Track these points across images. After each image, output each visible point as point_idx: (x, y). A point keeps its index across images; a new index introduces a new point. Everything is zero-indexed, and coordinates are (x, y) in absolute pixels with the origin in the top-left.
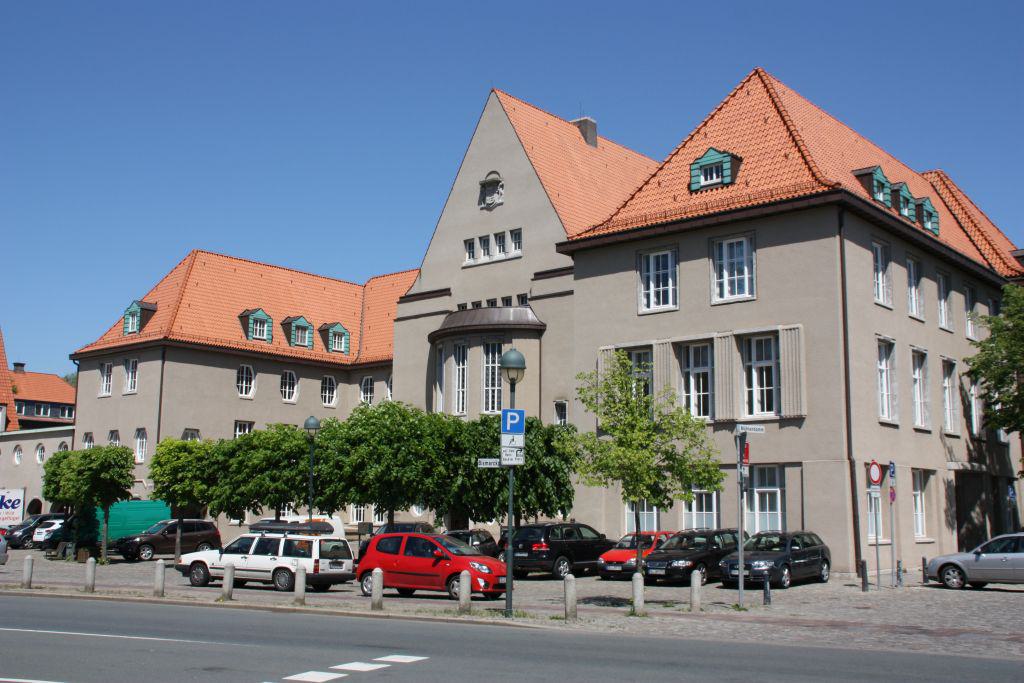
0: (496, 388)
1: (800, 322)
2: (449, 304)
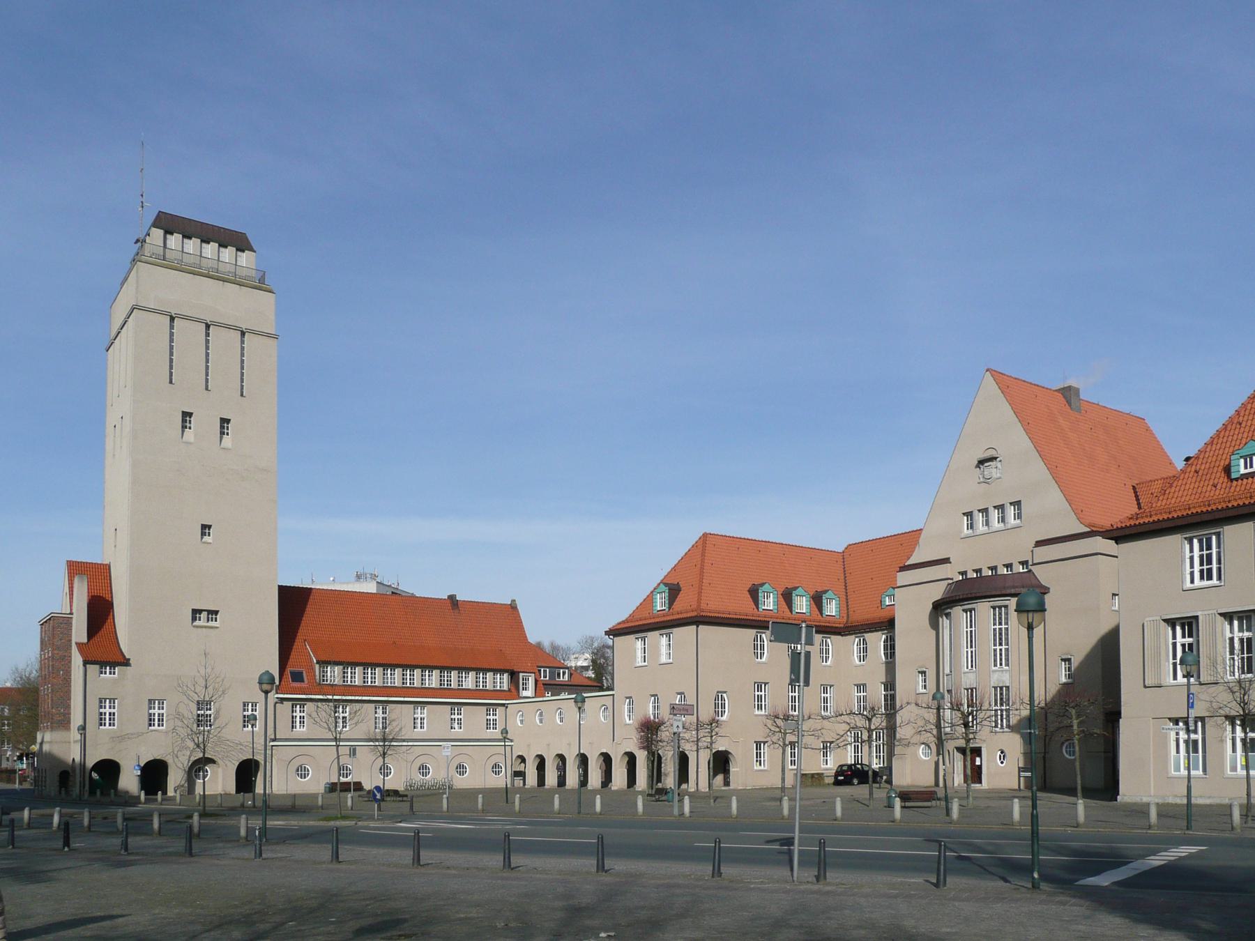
0: (1004, 647)
2: (951, 572)
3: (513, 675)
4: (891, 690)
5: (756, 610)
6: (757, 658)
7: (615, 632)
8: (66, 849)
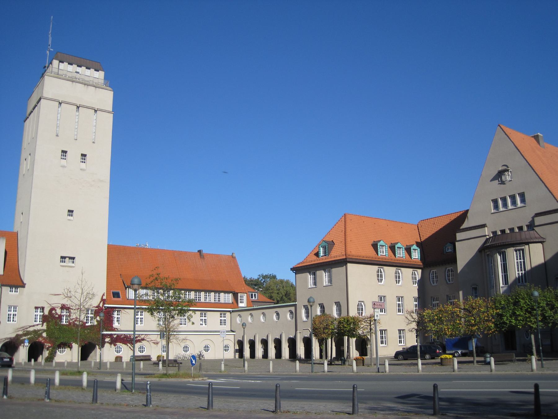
1: (257, 299)
2: (487, 231)
3: (235, 295)
4: (437, 301)
5: (377, 255)
6: (379, 282)
7: (297, 270)
8: (5, 397)
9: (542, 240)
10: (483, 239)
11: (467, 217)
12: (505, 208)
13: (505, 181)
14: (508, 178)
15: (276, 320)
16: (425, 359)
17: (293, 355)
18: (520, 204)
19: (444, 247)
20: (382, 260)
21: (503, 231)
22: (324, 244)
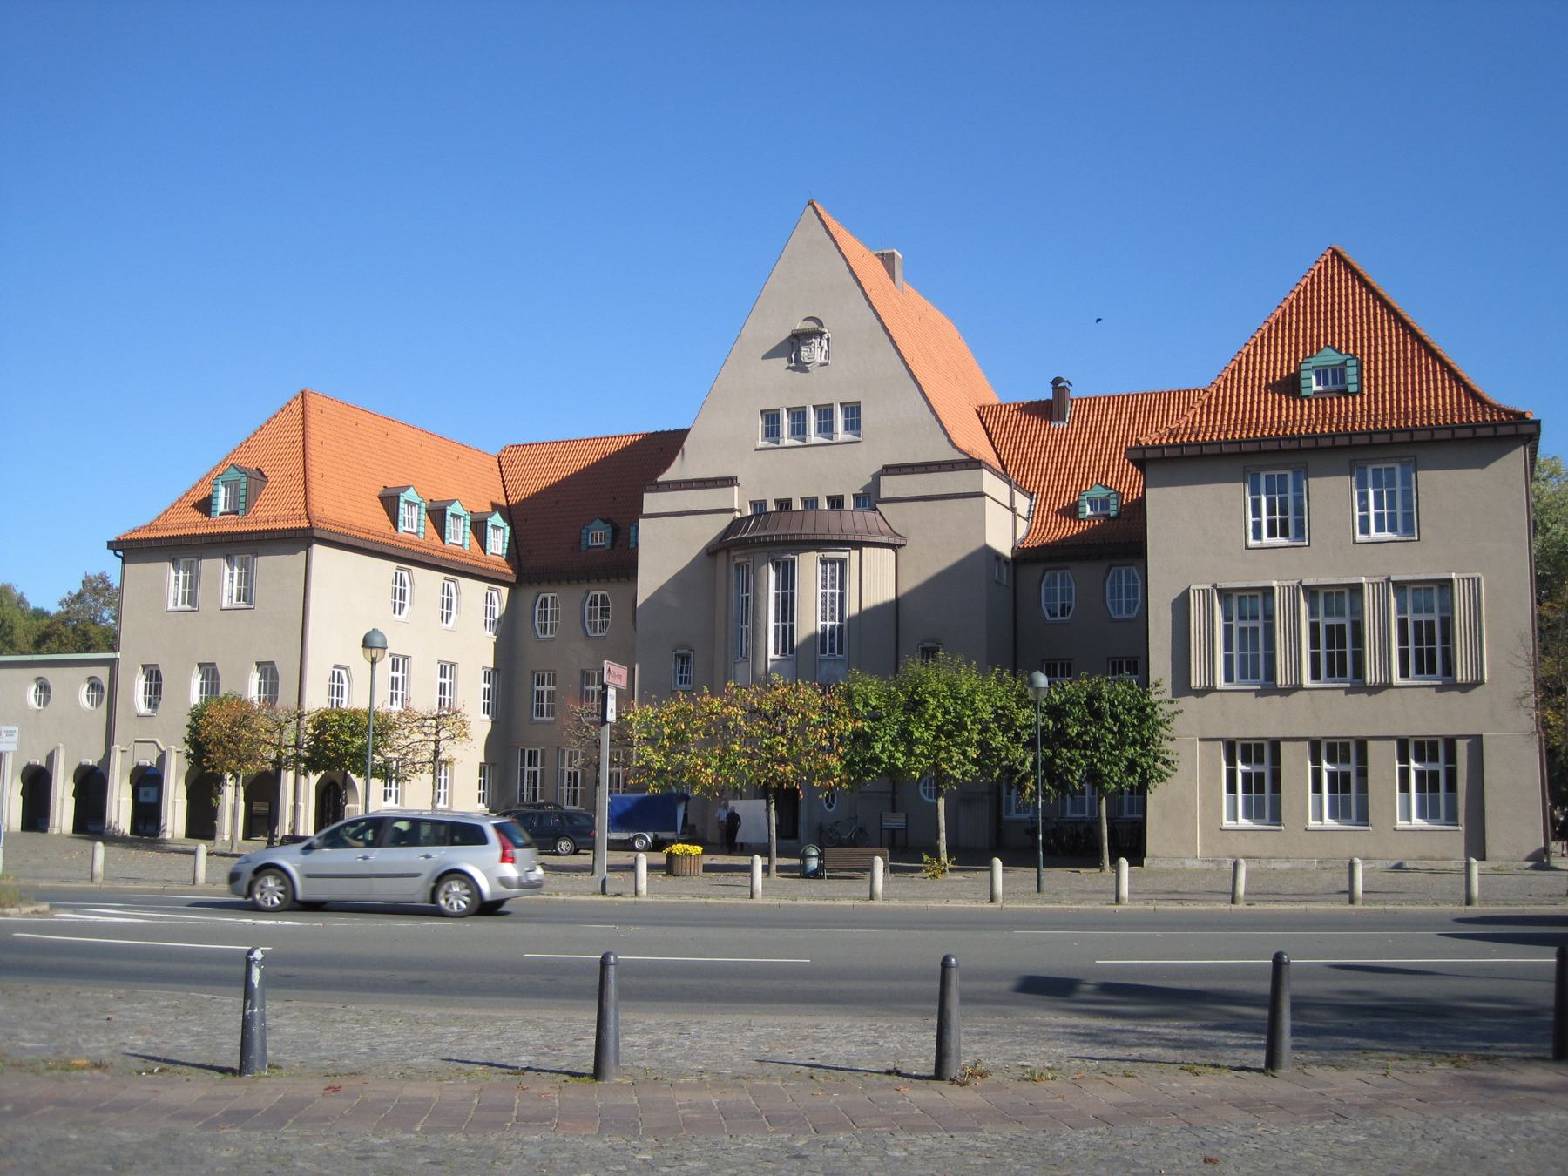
2: (737, 501)
4: (549, 685)
7: (130, 549)
9: (897, 541)
10: (726, 520)
11: (681, 452)
12: (798, 440)
13: (809, 363)
14: (819, 357)
15: (37, 707)
16: (557, 854)
17: (90, 817)
18: (844, 433)
19: (584, 531)
20: (410, 546)
21: (784, 504)
22: (234, 475)
